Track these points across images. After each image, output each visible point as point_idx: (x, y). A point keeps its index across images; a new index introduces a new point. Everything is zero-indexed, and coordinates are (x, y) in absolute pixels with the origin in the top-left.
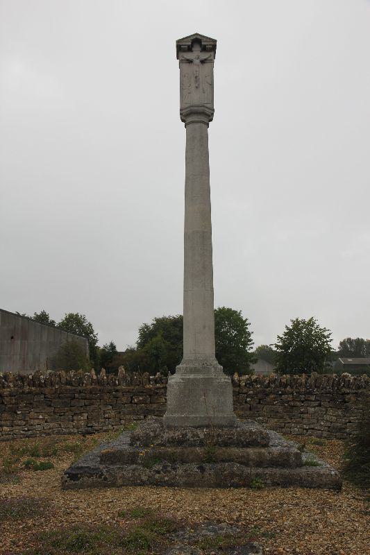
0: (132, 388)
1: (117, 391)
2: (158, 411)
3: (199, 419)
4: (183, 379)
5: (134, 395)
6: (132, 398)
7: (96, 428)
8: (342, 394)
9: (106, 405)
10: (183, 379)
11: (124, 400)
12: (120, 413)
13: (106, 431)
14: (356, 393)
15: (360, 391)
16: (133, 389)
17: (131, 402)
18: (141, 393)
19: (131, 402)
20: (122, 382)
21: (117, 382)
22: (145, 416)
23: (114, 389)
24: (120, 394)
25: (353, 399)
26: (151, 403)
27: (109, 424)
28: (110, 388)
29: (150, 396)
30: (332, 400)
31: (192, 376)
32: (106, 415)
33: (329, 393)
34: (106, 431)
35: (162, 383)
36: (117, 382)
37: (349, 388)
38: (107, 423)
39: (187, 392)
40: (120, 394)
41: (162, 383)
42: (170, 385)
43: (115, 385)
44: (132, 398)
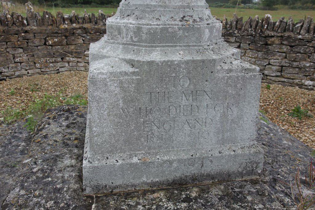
0: (44, 28)
1: (26, 32)
2: (76, 52)
3: (175, 165)
4: (131, 63)
5: (48, 36)
6: (45, 39)
7: (6, 74)
8: (266, 37)
9: (15, 48)
10: (131, 63)
11: (37, 42)
12: (33, 56)
13: (19, 76)
14: (282, 36)
15: (286, 34)
16: (46, 30)
17: (45, 44)
18: (54, 34)
19: (45, 44)
20: (31, 22)
21: (25, 22)
22: (62, 59)
23: (22, 29)
24: (31, 36)
25: (277, 42)
26: (67, 44)
27: (22, 68)
28: (16, 28)
29: (66, 37)
30: (253, 42)
31: (156, 56)
32: (17, 60)
33: (252, 35)
34: (19, 76)
35: (78, 22)
36: (25, 22)
37: (273, 30)
38: (19, 68)
39: (145, 99)
40: (31, 36)
41: (78, 22)
42: (94, 82)
43: (23, 24)
44: (45, 39)
